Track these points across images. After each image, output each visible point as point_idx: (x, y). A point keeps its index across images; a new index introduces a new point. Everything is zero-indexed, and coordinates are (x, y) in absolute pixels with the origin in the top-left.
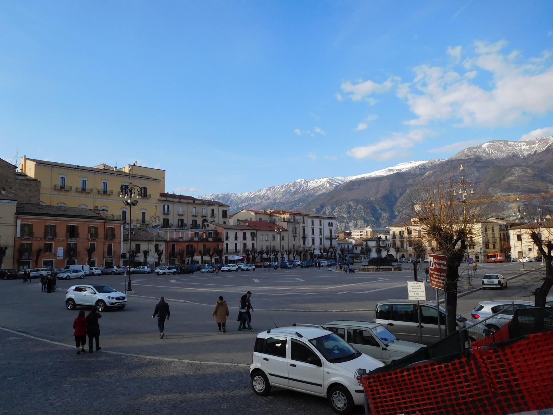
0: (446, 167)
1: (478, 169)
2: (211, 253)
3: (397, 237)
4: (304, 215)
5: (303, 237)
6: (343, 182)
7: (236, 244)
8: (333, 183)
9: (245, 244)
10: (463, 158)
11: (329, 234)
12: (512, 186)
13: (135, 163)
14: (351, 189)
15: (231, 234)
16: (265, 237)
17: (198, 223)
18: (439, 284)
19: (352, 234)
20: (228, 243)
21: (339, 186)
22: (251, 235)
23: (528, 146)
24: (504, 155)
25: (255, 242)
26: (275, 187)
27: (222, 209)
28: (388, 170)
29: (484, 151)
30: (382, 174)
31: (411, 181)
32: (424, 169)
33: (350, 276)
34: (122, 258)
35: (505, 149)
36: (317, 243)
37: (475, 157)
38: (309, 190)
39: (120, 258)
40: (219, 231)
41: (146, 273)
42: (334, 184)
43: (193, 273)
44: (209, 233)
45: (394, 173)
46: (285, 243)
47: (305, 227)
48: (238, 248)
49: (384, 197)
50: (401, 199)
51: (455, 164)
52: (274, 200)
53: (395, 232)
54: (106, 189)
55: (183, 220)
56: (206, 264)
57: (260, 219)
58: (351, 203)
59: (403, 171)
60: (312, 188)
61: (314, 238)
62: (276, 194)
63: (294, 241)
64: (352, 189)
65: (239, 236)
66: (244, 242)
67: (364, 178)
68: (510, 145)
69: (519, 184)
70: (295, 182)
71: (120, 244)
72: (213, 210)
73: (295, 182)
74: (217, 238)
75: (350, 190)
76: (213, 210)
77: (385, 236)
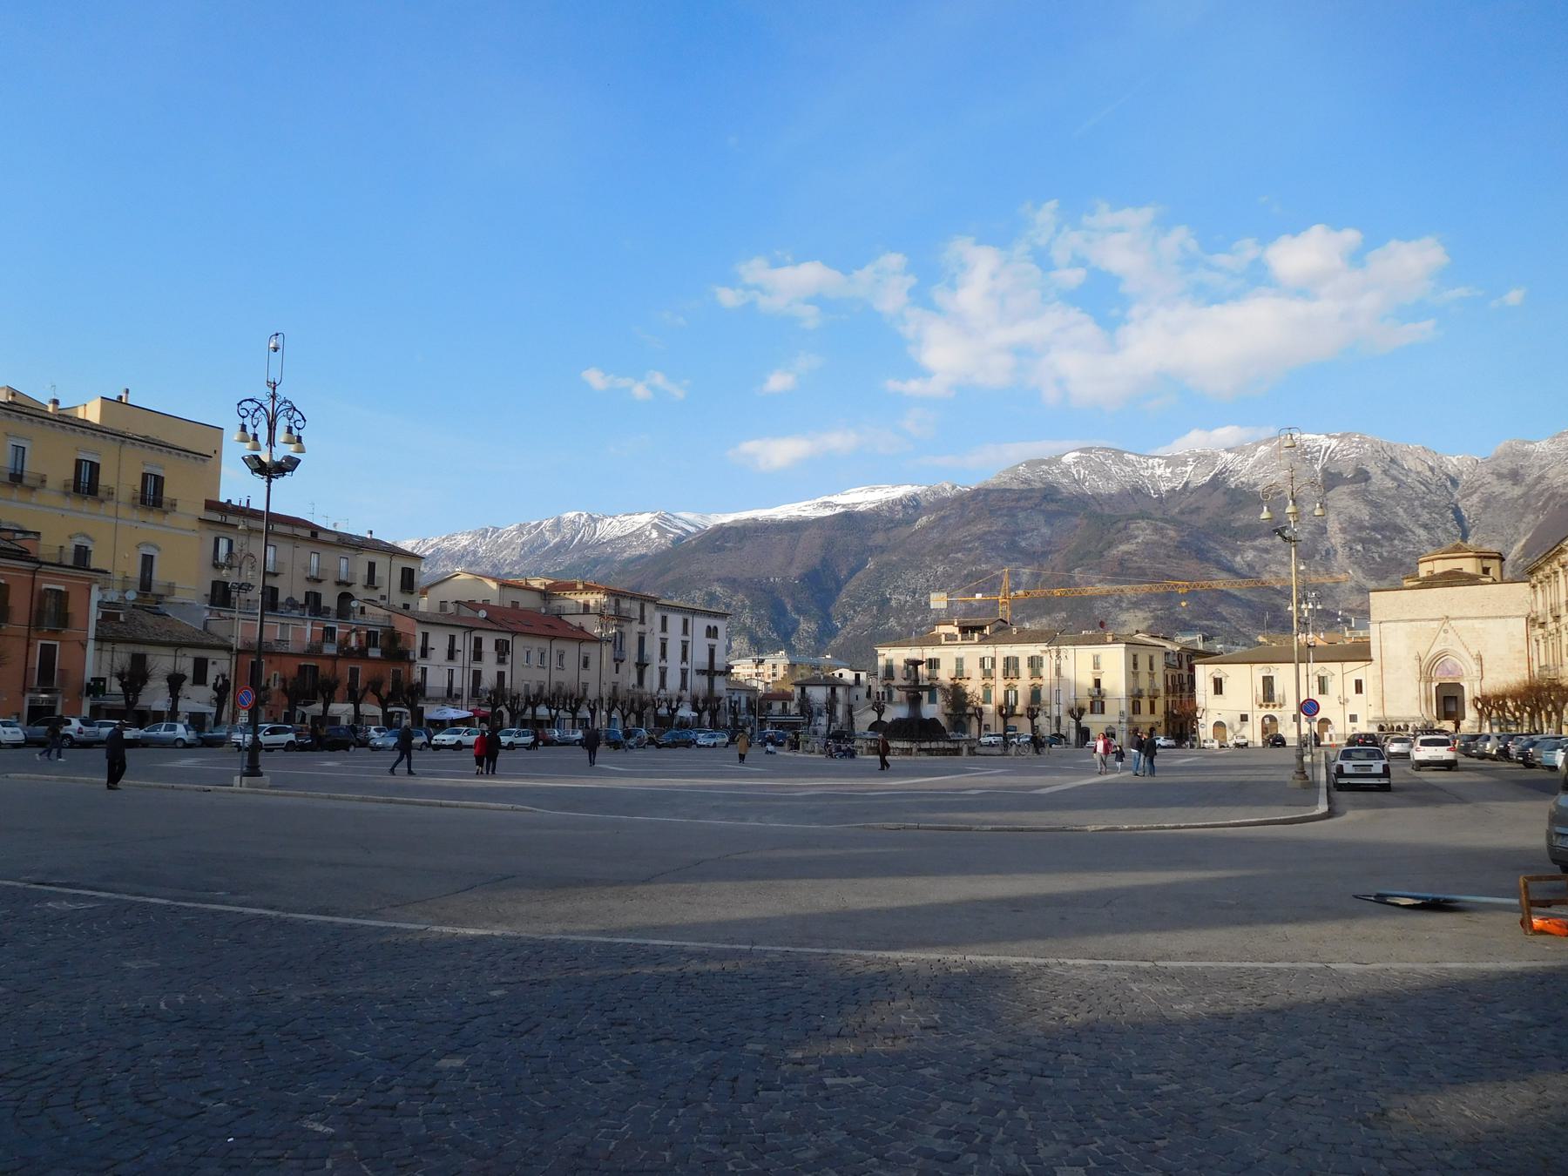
0: (971, 507)
1: (1050, 517)
2: (384, 692)
3: (899, 680)
4: (644, 600)
5: (637, 664)
6: (697, 527)
7: (451, 672)
8: (669, 528)
9: (477, 675)
10: (1015, 486)
11: (707, 660)
12: (1130, 568)
13: (124, 395)
14: (719, 550)
15: (438, 641)
16: (535, 655)
17: (324, 603)
18: (1544, 719)
19: (733, 671)
20: (426, 668)
21: (685, 538)
22: (496, 648)
23: (1170, 470)
24: (1113, 488)
25: (506, 669)
26: (498, 529)
27: (400, 563)
28: (822, 503)
29: (1066, 473)
30: (804, 514)
31: (879, 538)
32: (914, 507)
33: (846, 763)
34: (87, 695)
35: (1116, 472)
36: (673, 682)
37: (1043, 486)
38: (600, 544)
39: (80, 693)
41: (180, 746)
42: (672, 533)
43: (348, 750)
44: (369, 633)
45: (836, 512)
46: (590, 676)
47: (644, 633)
48: (457, 684)
49: (806, 575)
50: (851, 586)
51: (994, 500)
52: (494, 566)
53: (891, 660)
54: (19, 467)
55: (277, 589)
56: (373, 727)
57: (515, 604)
58: (718, 589)
59: (861, 508)
60: (608, 538)
61: (666, 668)
62: (500, 548)
63: (617, 672)
64: (721, 549)
65: (461, 648)
66: (476, 666)
67: (755, 520)
68: (1127, 463)
69: (1146, 564)
70: (559, 518)
71: (84, 646)
72: (372, 566)
73: (559, 518)
74: (395, 649)
75: (715, 552)
76: (372, 566)
77: (854, 673)
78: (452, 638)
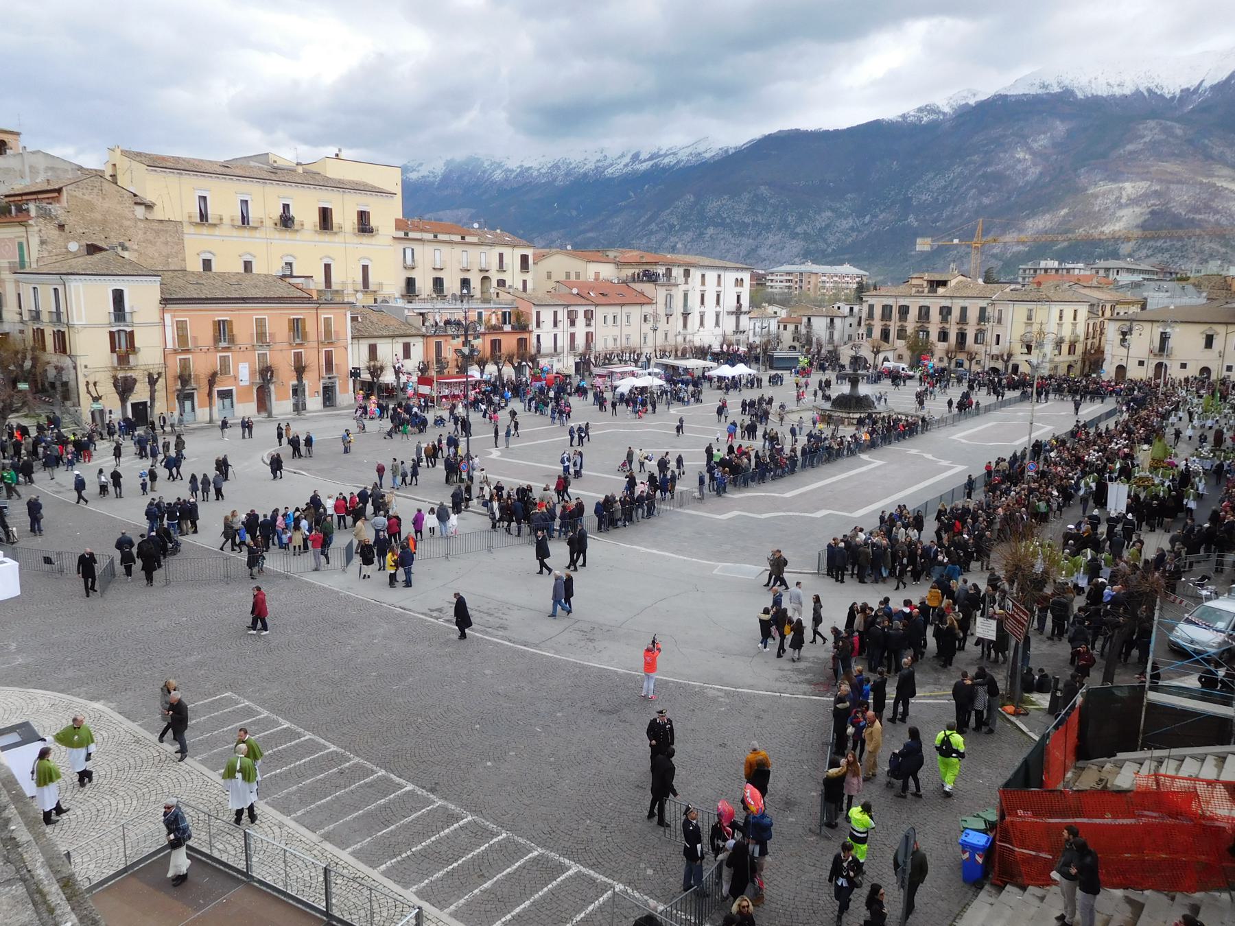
7: (555, 336)
15: (547, 315)
40: (521, 309)
58: (763, 190)
66: (572, 330)
71: (346, 349)
72: (501, 256)
76: (501, 256)
78: (555, 313)
